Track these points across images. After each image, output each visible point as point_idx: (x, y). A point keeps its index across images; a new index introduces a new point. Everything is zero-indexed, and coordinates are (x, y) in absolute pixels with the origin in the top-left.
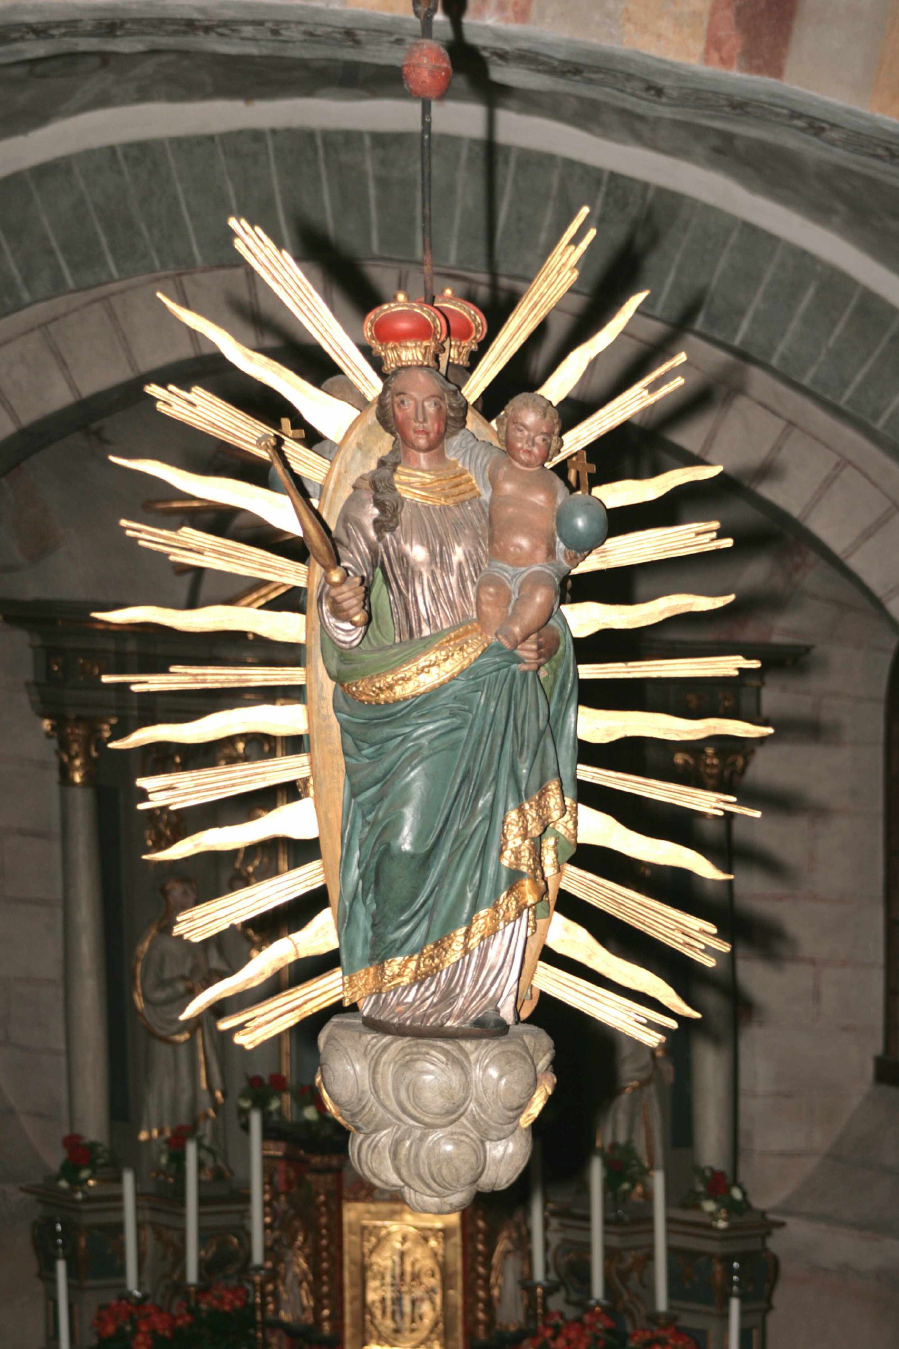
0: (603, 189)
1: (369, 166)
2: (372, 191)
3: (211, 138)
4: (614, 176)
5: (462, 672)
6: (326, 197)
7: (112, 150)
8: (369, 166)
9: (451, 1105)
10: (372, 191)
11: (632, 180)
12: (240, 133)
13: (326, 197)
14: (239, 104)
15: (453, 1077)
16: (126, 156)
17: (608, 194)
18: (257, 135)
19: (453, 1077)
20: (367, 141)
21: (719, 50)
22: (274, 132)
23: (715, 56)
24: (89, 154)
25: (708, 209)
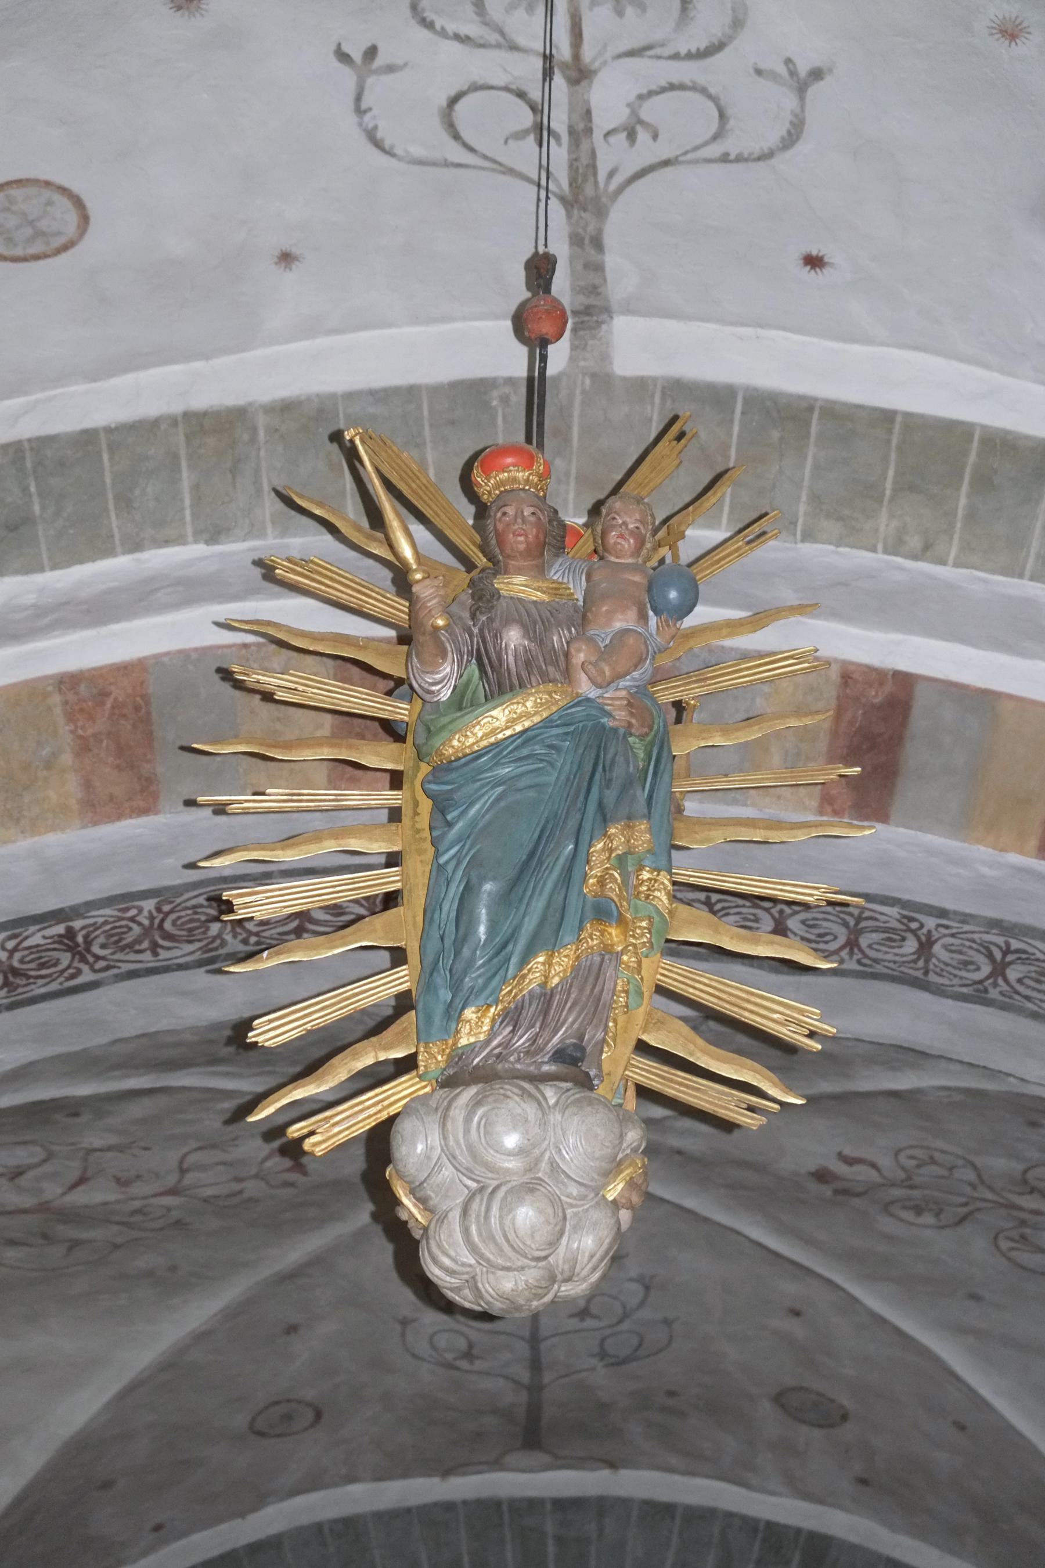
0: (760, 1535)
1: (550, 1528)
2: (551, 1548)
3: (409, 1510)
4: (769, 1525)
5: (547, 723)
6: (509, 1555)
7: (319, 1527)
8: (550, 1528)
9: (526, 1142)
10: (551, 1548)
11: (786, 1527)
12: (436, 1504)
13: (509, 1555)
14: (436, 1480)
15: (529, 1110)
16: (331, 1530)
17: (764, 1540)
18: (449, 1506)
19: (529, 1110)
20: (549, 1507)
21: (831, 804)
22: (465, 1502)
23: (829, 809)
24: (300, 1530)
25: (853, 1548)
